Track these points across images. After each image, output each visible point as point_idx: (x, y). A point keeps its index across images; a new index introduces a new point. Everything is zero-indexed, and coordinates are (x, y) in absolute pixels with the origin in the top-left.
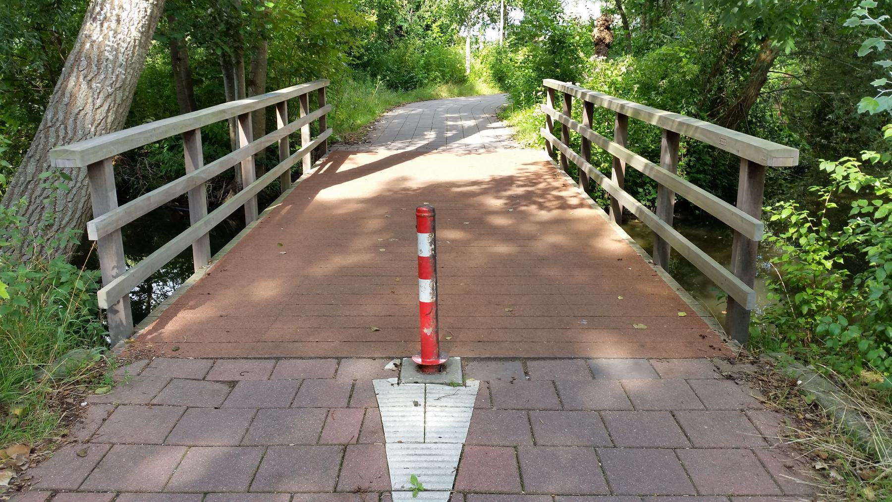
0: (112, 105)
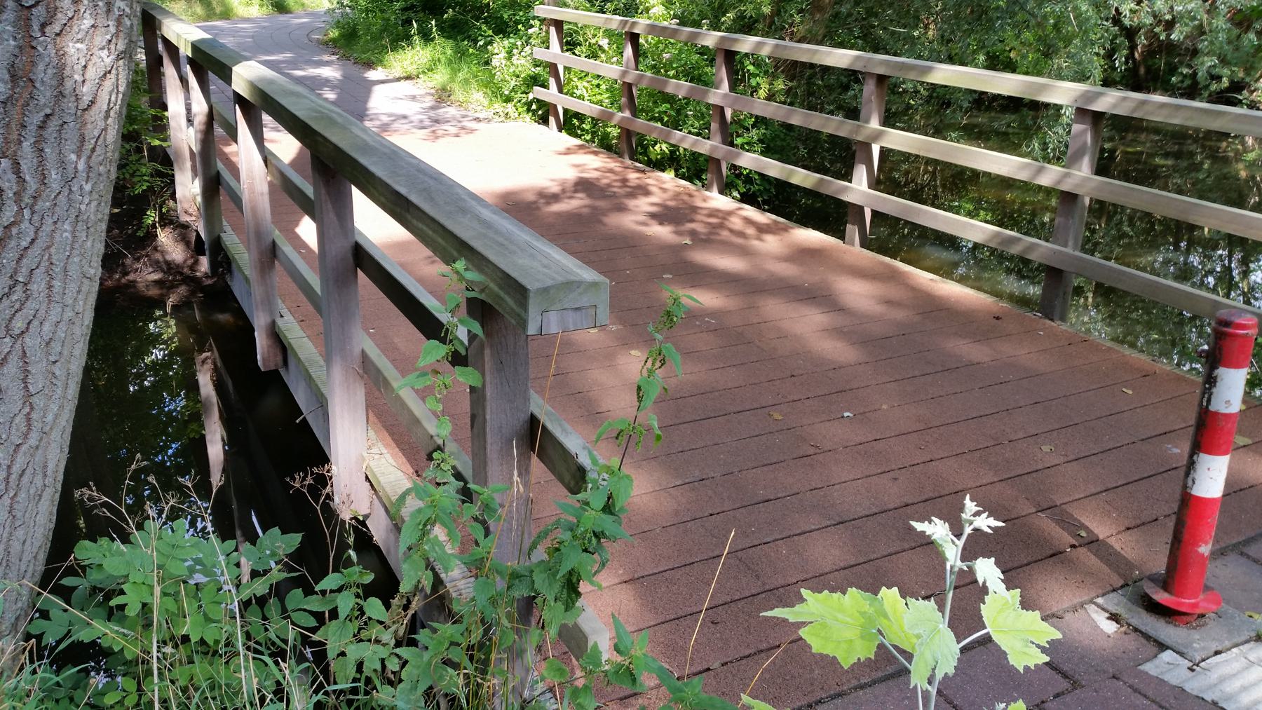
0: (113, 98)
